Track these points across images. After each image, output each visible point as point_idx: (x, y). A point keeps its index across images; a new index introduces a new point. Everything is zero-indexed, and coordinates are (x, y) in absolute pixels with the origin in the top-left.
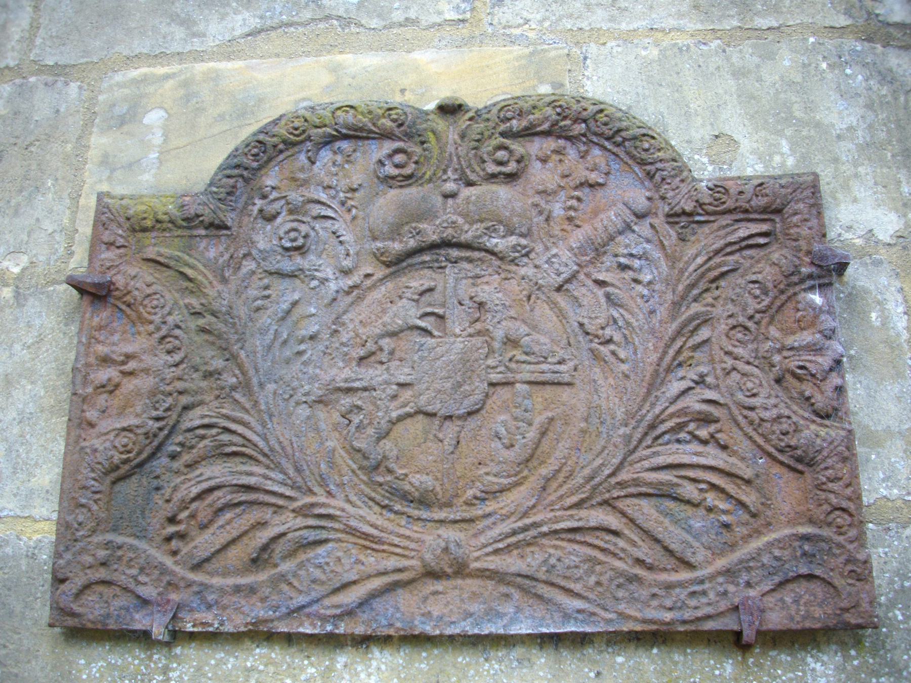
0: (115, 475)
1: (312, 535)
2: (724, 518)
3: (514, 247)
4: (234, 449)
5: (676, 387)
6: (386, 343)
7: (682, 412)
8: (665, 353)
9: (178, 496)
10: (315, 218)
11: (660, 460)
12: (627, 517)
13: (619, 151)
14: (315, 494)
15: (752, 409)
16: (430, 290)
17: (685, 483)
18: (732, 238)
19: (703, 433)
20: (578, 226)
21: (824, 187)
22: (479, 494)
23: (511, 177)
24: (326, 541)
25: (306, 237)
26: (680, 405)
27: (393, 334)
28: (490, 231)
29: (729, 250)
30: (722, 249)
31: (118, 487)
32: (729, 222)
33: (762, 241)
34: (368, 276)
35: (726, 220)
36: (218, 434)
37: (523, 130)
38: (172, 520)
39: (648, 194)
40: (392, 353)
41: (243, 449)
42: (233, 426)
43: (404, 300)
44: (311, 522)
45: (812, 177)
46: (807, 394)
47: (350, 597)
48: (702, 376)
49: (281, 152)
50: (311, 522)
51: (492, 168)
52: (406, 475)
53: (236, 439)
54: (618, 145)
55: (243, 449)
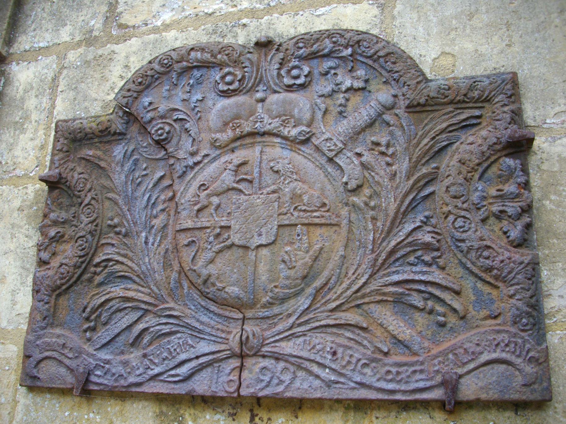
0: (57, 292)
1: (166, 329)
2: (441, 319)
3: (300, 133)
4: (123, 274)
5: (409, 227)
6: (215, 200)
7: (410, 244)
8: (402, 202)
9: (91, 306)
10: (175, 121)
11: (396, 278)
12: (198, 289)
13: (376, 65)
14: (167, 302)
15: (463, 241)
16: (244, 164)
17: (415, 294)
18: (454, 120)
19: (427, 258)
20: (345, 117)
21: (521, 79)
22: (270, 300)
23: (303, 86)
24: (177, 332)
25: (168, 133)
26: (410, 239)
27: (218, 195)
28: (284, 123)
29: (451, 129)
30: (446, 128)
31: (61, 300)
32: (452, 109)
33: (474, 121)
34: (207, 155)
35: (450, 108)
36: (114, 265)
37: (309, 54)
38: (87, 319)
39: (393, 92)
40: (218, 206)
41: (127, 274)
42: (124, 260)
43: (227, 171)
44: (164, 320)
45: (511, 75)
46: (505, 229)
47: (184, 370)
48: (427, 218)
49: (157, 79)
50: (164, 320)
51: (287, 81)
52: (224, 288)
53: (124, 267)
54: (375, 61)
55: (127, 274)
